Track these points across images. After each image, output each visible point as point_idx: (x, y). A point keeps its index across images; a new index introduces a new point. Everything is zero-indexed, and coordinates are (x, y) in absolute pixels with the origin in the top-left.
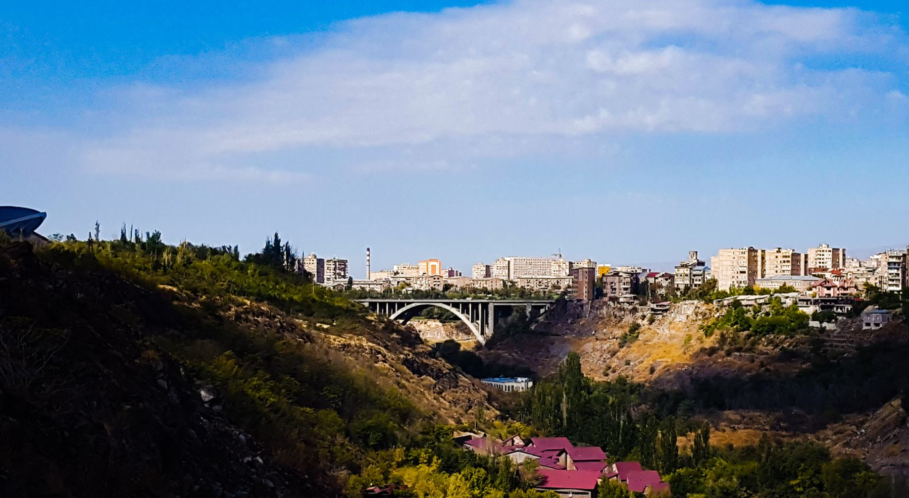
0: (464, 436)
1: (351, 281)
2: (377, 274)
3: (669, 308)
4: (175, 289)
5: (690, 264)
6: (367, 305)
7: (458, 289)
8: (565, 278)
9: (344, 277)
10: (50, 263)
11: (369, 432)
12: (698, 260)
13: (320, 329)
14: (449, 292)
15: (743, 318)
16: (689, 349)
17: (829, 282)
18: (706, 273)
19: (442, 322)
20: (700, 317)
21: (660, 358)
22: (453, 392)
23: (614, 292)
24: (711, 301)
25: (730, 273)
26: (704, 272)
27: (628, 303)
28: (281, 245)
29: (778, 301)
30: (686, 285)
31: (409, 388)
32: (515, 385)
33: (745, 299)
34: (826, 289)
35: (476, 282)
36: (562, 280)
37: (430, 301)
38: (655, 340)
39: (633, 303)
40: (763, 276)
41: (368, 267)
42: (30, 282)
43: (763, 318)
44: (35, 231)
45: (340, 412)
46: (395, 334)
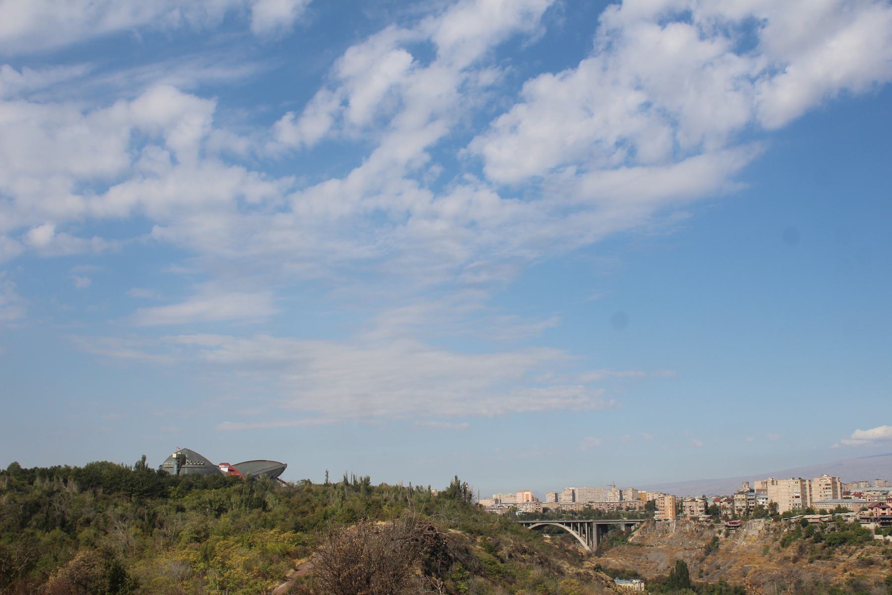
17: (883, 504)
18: (757, 498)
20: (772, 532)
23: (692, 513)
25: (787, 498)
26: (756, 497)
27: (706, 521)
34: (881, 510)
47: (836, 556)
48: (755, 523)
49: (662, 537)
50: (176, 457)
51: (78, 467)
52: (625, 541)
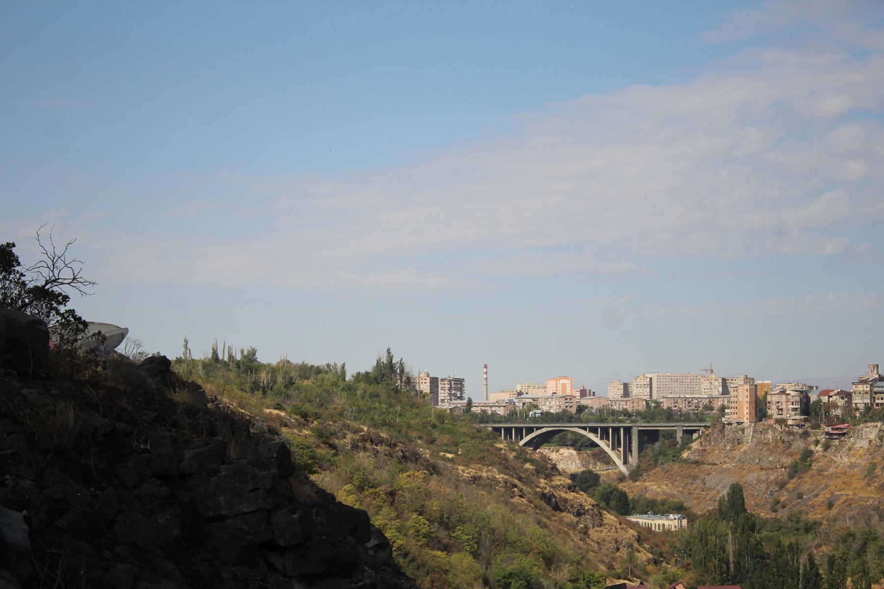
0: (617, 584)
1: (470, 403)
2: (497, 394)
4: (283, 414)
5: (870, 380)
6: (490, 429)
7: (594, 411)
8: (718, 398)
9: (461, 398)
11: (510, 580)
12: (879, 375)
13: (444, 459)
14: (584, 415)
16: (874, 480)
19: (578, 450)
21: (839, 491)
22: (597, 531)
27: (798, 426)
28: (394, 361)
30: (865, 404)
32: (667, 523)
35: (614, 403)
36: (715, 399)
37: (563, 425)
39: (804, 425)
41: (485, 386)
44: (115, 349)
45: (476, 555)
48: (868, 429)
49: (731, 450)
52: (676, 458)
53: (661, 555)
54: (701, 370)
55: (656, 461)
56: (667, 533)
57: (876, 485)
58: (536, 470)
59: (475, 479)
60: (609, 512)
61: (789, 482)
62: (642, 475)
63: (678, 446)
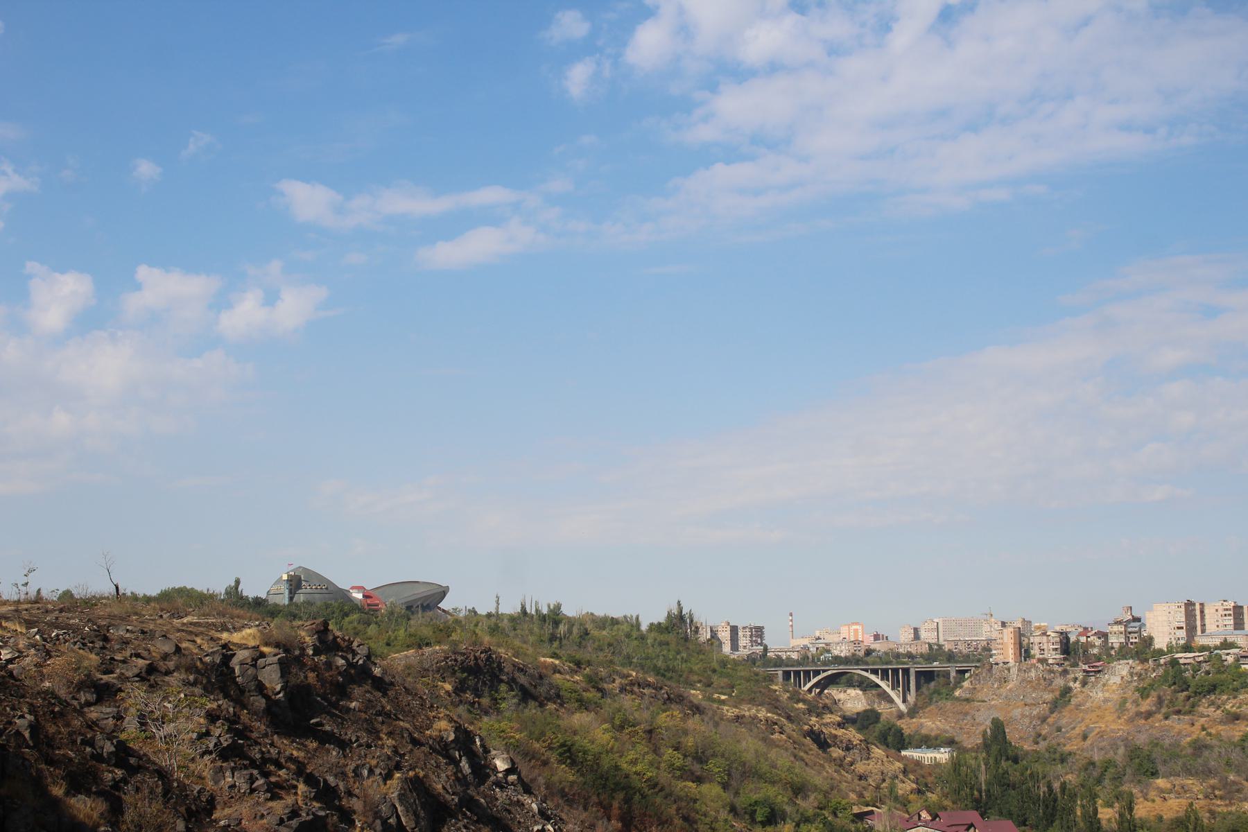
1: (766, 649)
3: (1102, 669)
4: (557, 662)
9: (761, 644)
10: (352, 639)
11: (756, 808)
12: (1133, 616)
15: (1181, 679)
18: (1142, 630)
19: (864, 690)
20: (1135, 678)
21: (1093, 724)
22: (865, 764)
24: (1146, 660)
27: (1058, 664)
29: (1218, 659)
31: (807, 760)
32: (938, 756)
33: (1183, 657)
38: (1088, 705)
40: (1203, 631)
42: (322, 658)
43: (1202, 677)
44: (439, 605)
45: (725, 786)
46: (801, 704)
47: (1201, 709)
50: (286, 578)
51: (148, 595)
52: (949, 696)
53: (926, 785)
54: (982, 614)
55: (931, 699)
56: (937, 765)
57: (1125, 717)
58: (808, 709)
59: (738, 719)
60: (877, 747)
61: (1050, 717)
62: (918, 712)
63: (951, 685)
